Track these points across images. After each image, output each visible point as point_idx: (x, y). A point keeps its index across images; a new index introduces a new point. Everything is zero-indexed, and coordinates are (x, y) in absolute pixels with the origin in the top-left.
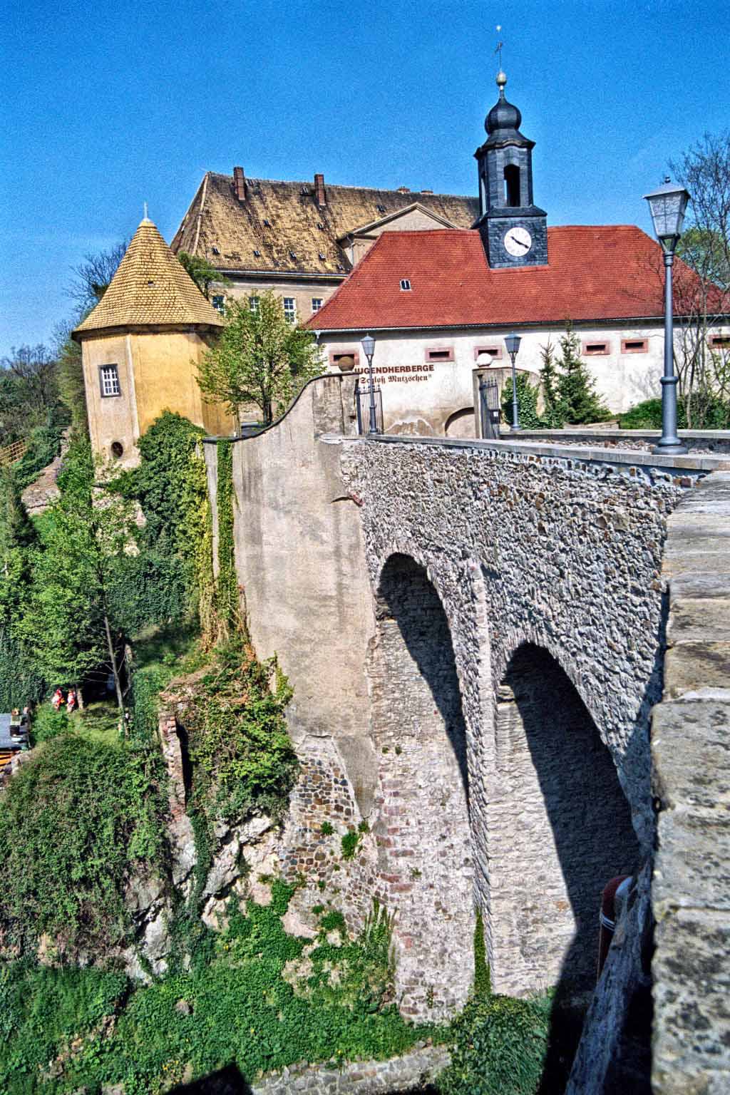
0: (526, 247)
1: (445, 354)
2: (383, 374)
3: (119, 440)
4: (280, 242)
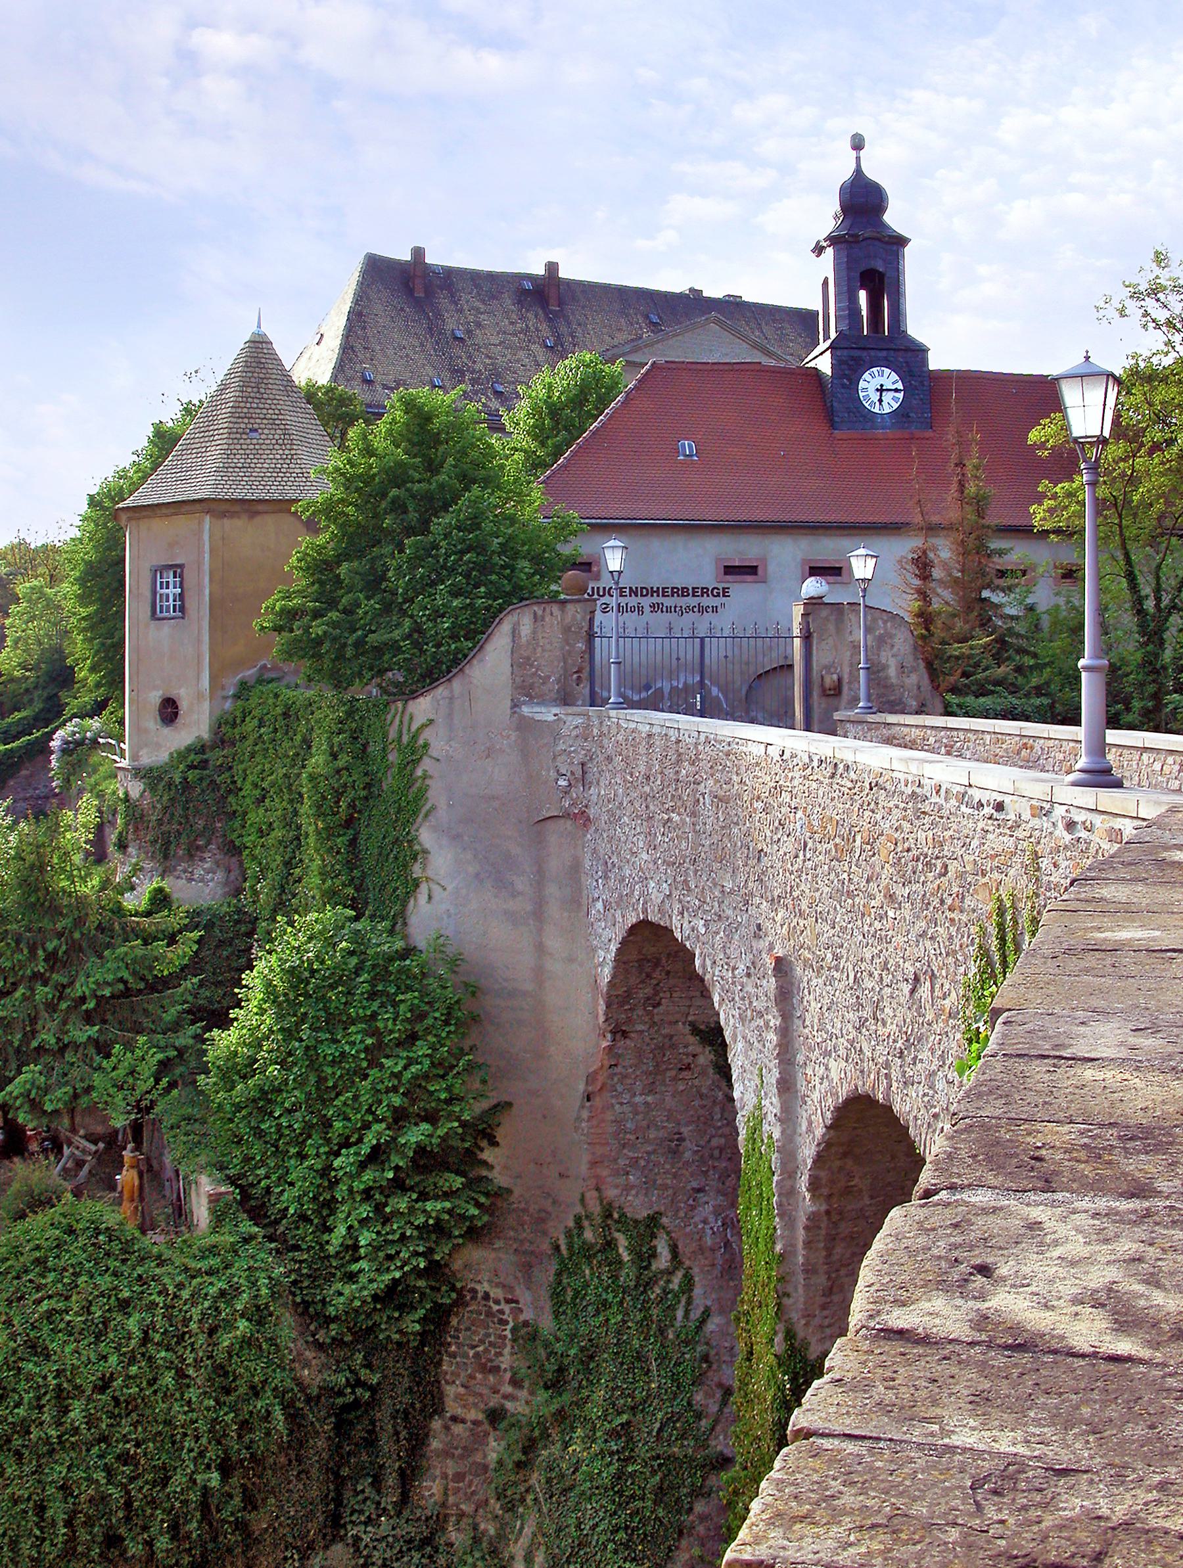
0: (896, 390)
1: (752, 570)
2: (639, 599)
3: (172, 694)
4: (477, 367)
